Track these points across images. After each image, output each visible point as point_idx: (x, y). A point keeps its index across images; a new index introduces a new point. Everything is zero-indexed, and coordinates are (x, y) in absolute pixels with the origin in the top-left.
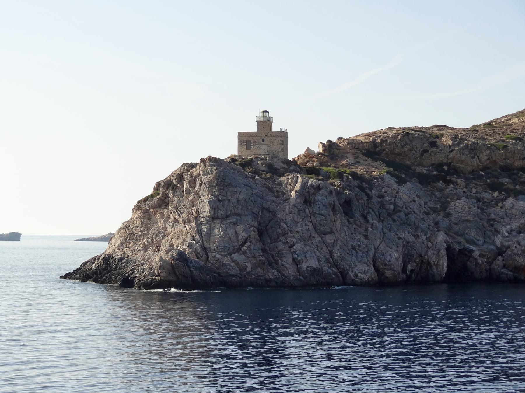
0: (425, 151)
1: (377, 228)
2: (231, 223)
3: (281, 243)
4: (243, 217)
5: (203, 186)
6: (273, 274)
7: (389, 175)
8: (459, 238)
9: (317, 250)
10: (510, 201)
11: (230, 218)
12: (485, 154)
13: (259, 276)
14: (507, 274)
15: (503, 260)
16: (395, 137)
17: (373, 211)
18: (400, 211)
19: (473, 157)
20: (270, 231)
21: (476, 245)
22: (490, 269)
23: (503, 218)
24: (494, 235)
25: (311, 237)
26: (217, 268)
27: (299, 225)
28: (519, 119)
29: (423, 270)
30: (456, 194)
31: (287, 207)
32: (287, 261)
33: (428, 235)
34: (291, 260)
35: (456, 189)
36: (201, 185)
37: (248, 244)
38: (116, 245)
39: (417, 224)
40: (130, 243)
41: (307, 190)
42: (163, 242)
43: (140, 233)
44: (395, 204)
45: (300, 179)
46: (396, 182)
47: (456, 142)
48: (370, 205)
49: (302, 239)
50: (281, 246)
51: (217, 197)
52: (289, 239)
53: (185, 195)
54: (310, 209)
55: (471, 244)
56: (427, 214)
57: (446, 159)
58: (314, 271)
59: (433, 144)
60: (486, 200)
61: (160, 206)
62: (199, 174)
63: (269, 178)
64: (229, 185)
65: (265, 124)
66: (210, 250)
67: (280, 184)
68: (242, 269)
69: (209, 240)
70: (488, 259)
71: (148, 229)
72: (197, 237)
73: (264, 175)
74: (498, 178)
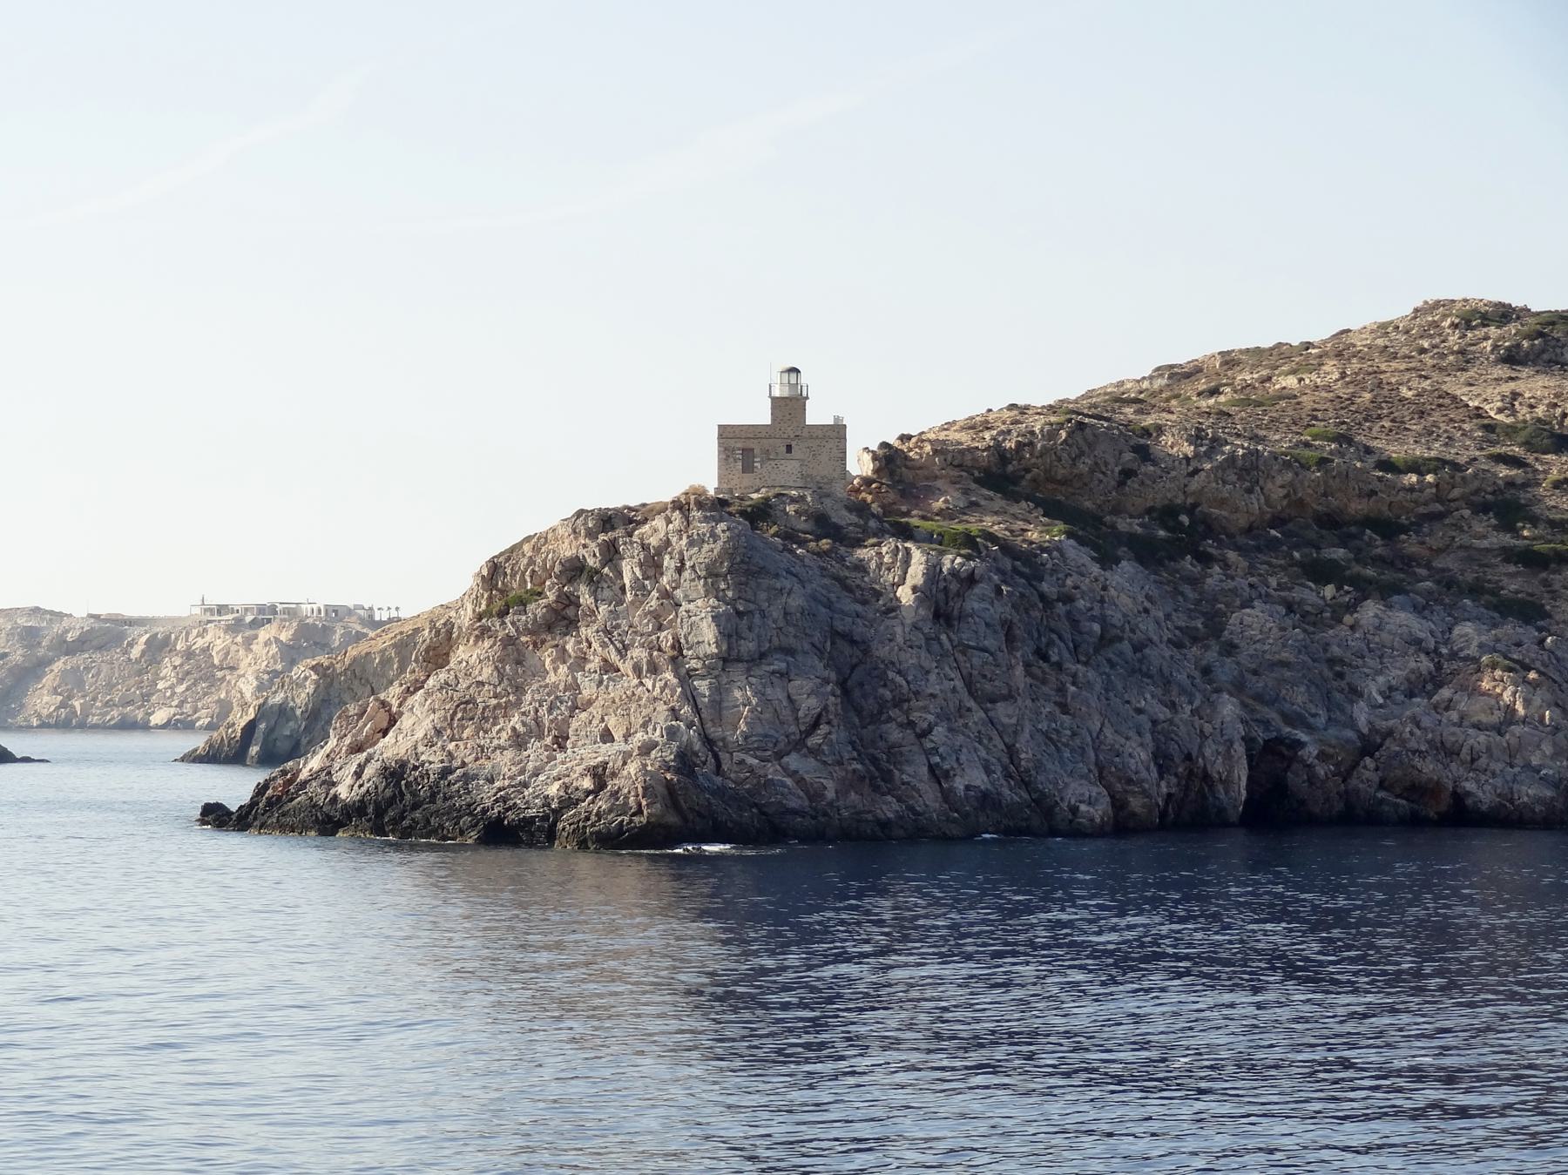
0: (1128, 474)
1: (1089, 685)
2: (773, 673)
3: (893, 725)
4: (800, 658)
5: (687, 574)
6: (889, 808)
7: (1072, 542)
8: (1266, 709)
9: (980, 742)
10: (1370, 611)
11: (770, 659)
12: (1279, 480)
13: (859, 813)
14: (1396, 805)
15: (1377, 769)
16: (1052, 434)
17: (1061, 638)
18: (1121, 639)
19: (1250, 491)
20: (857, 693)
21: (1310, 728)
22: (1346, 792)
23: (1363, 657)
24: (1352, 702)
25: (962, 711)
26: (748, 791)
27: (932, 677)
28: (1300, 380)
29: (1192, 795)
30: (1234, 591)
31: (899, 630)
32: (915, 771)
33: (1197, 703)
34: (925, 769)
35: (1233, 578)
36: (680, 570)
37: (824, 729)
38: (420, 734)
39: (1166, 673)
40: (464, 728)
41: (942, 585)
42: (574, 724)
43: (494, 702)
44: (1103, 620)
45: (917, 557)
46: (1093, 558)
47: (1203, 449)
48: (1052, 624)
49: (944, 716)
50: (895, 734)
51: (732, 602)
52: (915, 716)
53: (629, 597)
54: (953, 637)
55: (1295, 727)
56: (1178, 645)
57: (1182, 497)
58: (986, 800)
59: (1144, 453)
60: (1309, 608)
61: (549, 628)
62: (668, 543)
63: (826, 553)
64: (762, 571)
65: (790, 406)
66: (725, 746)
67: (861, 567)
68: (815, 795)
69: (719, 718)
70: (1337, 765)
71: (519, 690)
72: (686, 710)
73: (813, 544)
74: (1318, 548)
